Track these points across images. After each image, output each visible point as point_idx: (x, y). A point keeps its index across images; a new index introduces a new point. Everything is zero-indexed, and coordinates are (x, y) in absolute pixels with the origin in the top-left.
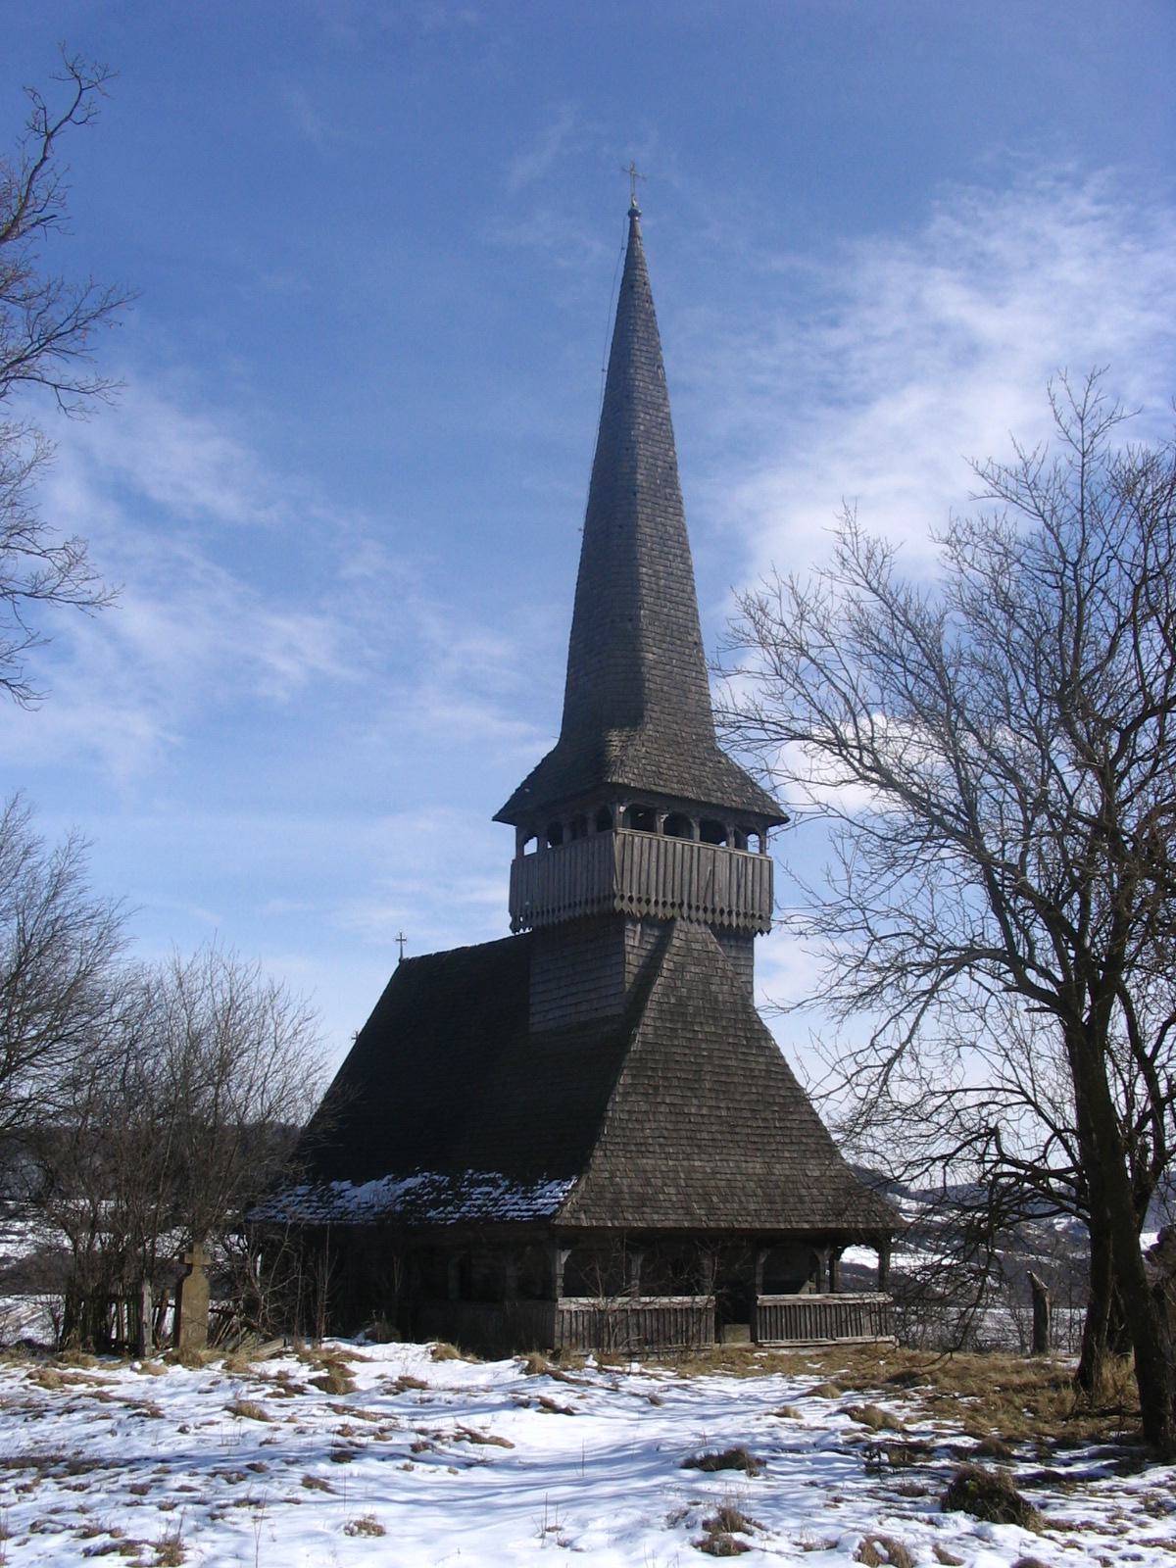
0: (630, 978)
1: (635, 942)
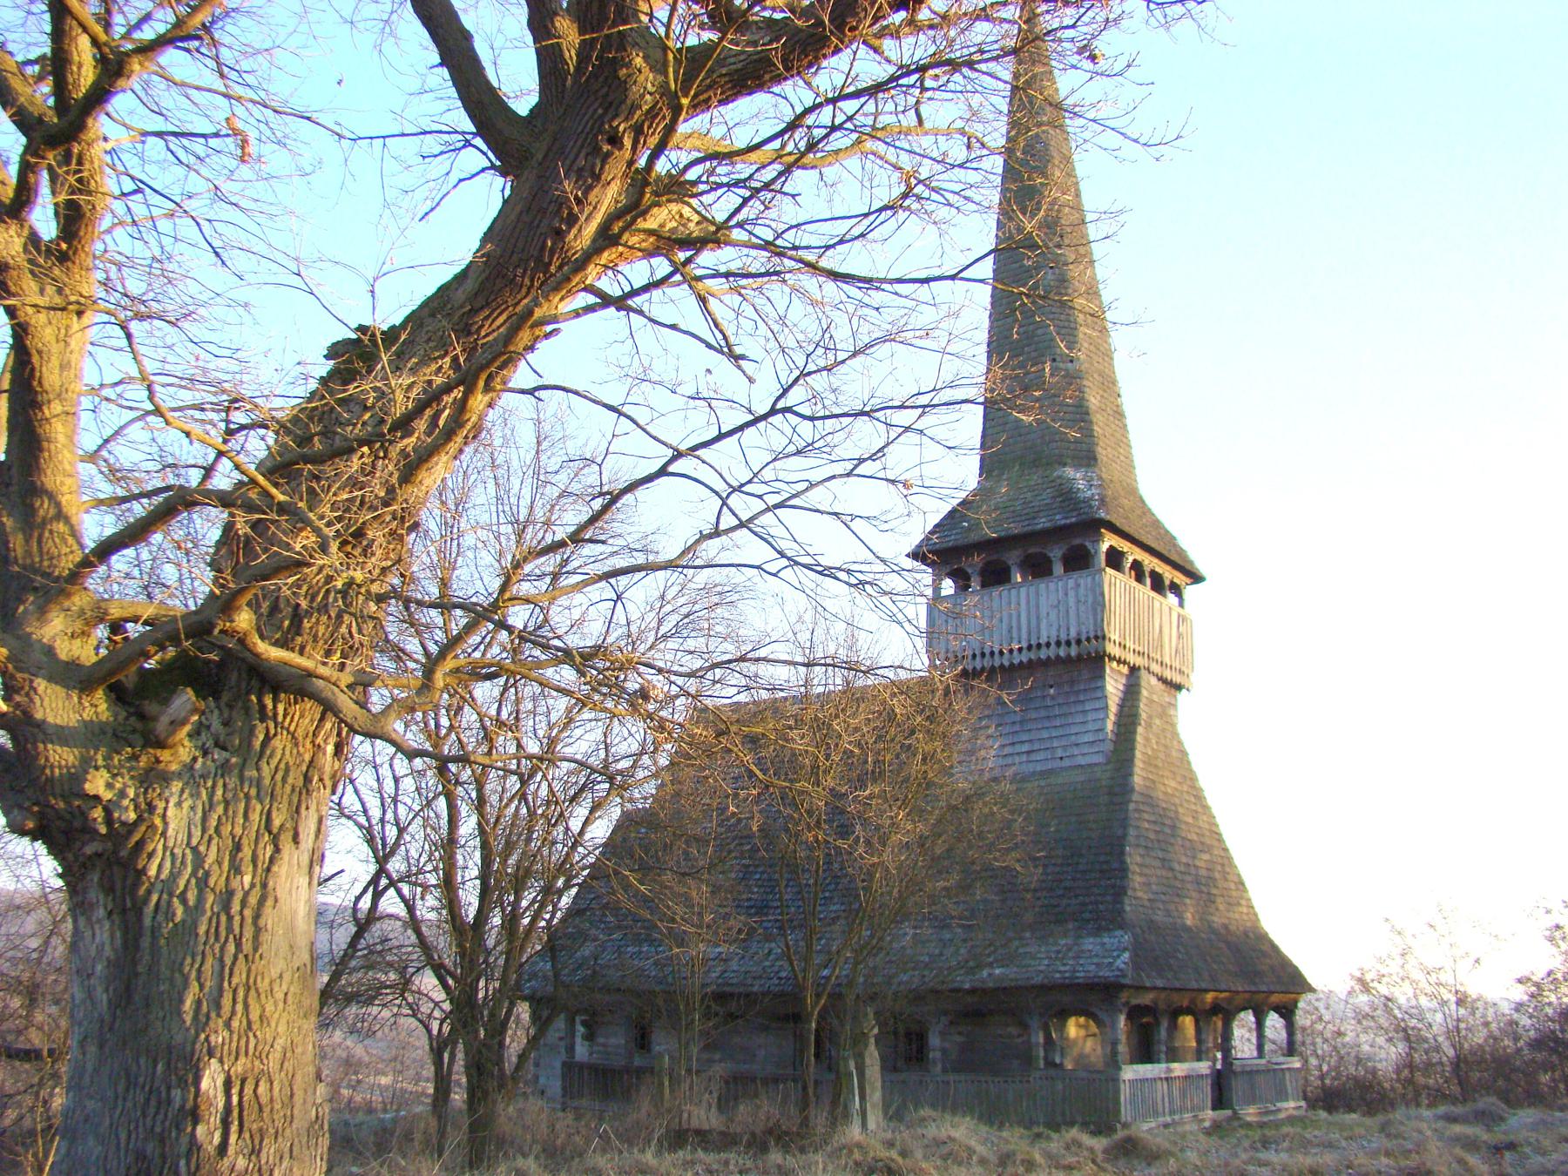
0: (1109, 726)
1: (1113, 686)
